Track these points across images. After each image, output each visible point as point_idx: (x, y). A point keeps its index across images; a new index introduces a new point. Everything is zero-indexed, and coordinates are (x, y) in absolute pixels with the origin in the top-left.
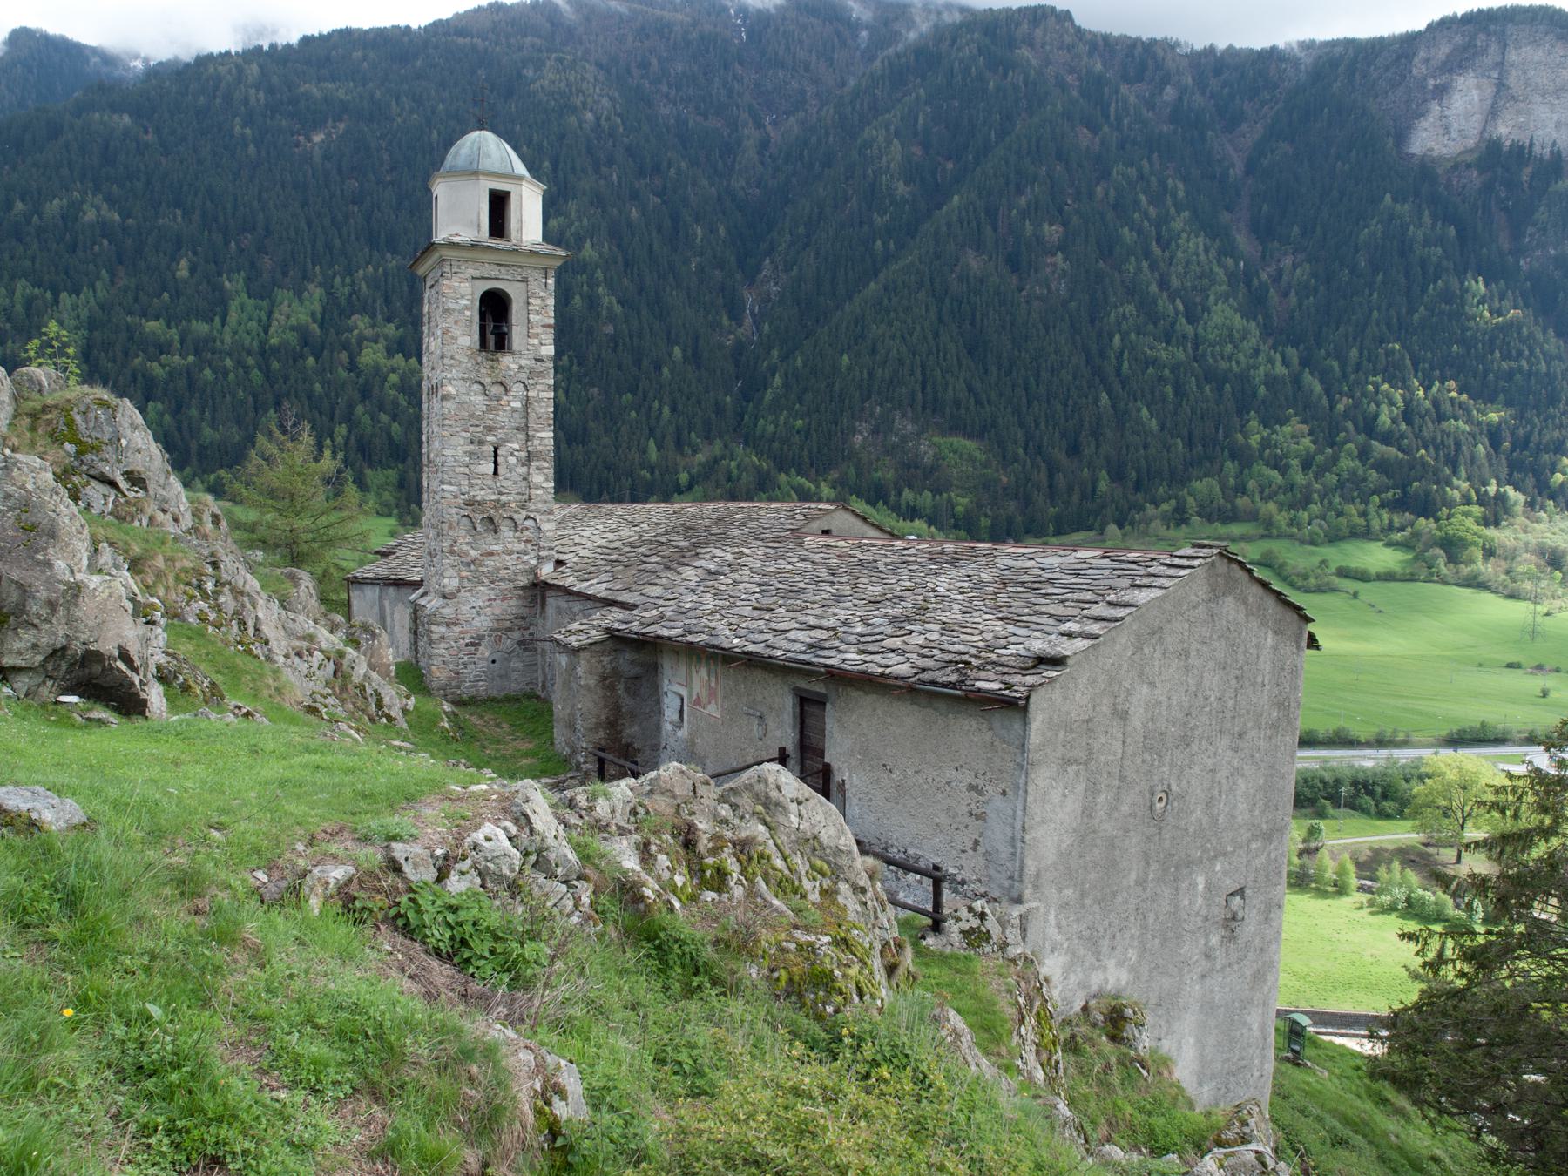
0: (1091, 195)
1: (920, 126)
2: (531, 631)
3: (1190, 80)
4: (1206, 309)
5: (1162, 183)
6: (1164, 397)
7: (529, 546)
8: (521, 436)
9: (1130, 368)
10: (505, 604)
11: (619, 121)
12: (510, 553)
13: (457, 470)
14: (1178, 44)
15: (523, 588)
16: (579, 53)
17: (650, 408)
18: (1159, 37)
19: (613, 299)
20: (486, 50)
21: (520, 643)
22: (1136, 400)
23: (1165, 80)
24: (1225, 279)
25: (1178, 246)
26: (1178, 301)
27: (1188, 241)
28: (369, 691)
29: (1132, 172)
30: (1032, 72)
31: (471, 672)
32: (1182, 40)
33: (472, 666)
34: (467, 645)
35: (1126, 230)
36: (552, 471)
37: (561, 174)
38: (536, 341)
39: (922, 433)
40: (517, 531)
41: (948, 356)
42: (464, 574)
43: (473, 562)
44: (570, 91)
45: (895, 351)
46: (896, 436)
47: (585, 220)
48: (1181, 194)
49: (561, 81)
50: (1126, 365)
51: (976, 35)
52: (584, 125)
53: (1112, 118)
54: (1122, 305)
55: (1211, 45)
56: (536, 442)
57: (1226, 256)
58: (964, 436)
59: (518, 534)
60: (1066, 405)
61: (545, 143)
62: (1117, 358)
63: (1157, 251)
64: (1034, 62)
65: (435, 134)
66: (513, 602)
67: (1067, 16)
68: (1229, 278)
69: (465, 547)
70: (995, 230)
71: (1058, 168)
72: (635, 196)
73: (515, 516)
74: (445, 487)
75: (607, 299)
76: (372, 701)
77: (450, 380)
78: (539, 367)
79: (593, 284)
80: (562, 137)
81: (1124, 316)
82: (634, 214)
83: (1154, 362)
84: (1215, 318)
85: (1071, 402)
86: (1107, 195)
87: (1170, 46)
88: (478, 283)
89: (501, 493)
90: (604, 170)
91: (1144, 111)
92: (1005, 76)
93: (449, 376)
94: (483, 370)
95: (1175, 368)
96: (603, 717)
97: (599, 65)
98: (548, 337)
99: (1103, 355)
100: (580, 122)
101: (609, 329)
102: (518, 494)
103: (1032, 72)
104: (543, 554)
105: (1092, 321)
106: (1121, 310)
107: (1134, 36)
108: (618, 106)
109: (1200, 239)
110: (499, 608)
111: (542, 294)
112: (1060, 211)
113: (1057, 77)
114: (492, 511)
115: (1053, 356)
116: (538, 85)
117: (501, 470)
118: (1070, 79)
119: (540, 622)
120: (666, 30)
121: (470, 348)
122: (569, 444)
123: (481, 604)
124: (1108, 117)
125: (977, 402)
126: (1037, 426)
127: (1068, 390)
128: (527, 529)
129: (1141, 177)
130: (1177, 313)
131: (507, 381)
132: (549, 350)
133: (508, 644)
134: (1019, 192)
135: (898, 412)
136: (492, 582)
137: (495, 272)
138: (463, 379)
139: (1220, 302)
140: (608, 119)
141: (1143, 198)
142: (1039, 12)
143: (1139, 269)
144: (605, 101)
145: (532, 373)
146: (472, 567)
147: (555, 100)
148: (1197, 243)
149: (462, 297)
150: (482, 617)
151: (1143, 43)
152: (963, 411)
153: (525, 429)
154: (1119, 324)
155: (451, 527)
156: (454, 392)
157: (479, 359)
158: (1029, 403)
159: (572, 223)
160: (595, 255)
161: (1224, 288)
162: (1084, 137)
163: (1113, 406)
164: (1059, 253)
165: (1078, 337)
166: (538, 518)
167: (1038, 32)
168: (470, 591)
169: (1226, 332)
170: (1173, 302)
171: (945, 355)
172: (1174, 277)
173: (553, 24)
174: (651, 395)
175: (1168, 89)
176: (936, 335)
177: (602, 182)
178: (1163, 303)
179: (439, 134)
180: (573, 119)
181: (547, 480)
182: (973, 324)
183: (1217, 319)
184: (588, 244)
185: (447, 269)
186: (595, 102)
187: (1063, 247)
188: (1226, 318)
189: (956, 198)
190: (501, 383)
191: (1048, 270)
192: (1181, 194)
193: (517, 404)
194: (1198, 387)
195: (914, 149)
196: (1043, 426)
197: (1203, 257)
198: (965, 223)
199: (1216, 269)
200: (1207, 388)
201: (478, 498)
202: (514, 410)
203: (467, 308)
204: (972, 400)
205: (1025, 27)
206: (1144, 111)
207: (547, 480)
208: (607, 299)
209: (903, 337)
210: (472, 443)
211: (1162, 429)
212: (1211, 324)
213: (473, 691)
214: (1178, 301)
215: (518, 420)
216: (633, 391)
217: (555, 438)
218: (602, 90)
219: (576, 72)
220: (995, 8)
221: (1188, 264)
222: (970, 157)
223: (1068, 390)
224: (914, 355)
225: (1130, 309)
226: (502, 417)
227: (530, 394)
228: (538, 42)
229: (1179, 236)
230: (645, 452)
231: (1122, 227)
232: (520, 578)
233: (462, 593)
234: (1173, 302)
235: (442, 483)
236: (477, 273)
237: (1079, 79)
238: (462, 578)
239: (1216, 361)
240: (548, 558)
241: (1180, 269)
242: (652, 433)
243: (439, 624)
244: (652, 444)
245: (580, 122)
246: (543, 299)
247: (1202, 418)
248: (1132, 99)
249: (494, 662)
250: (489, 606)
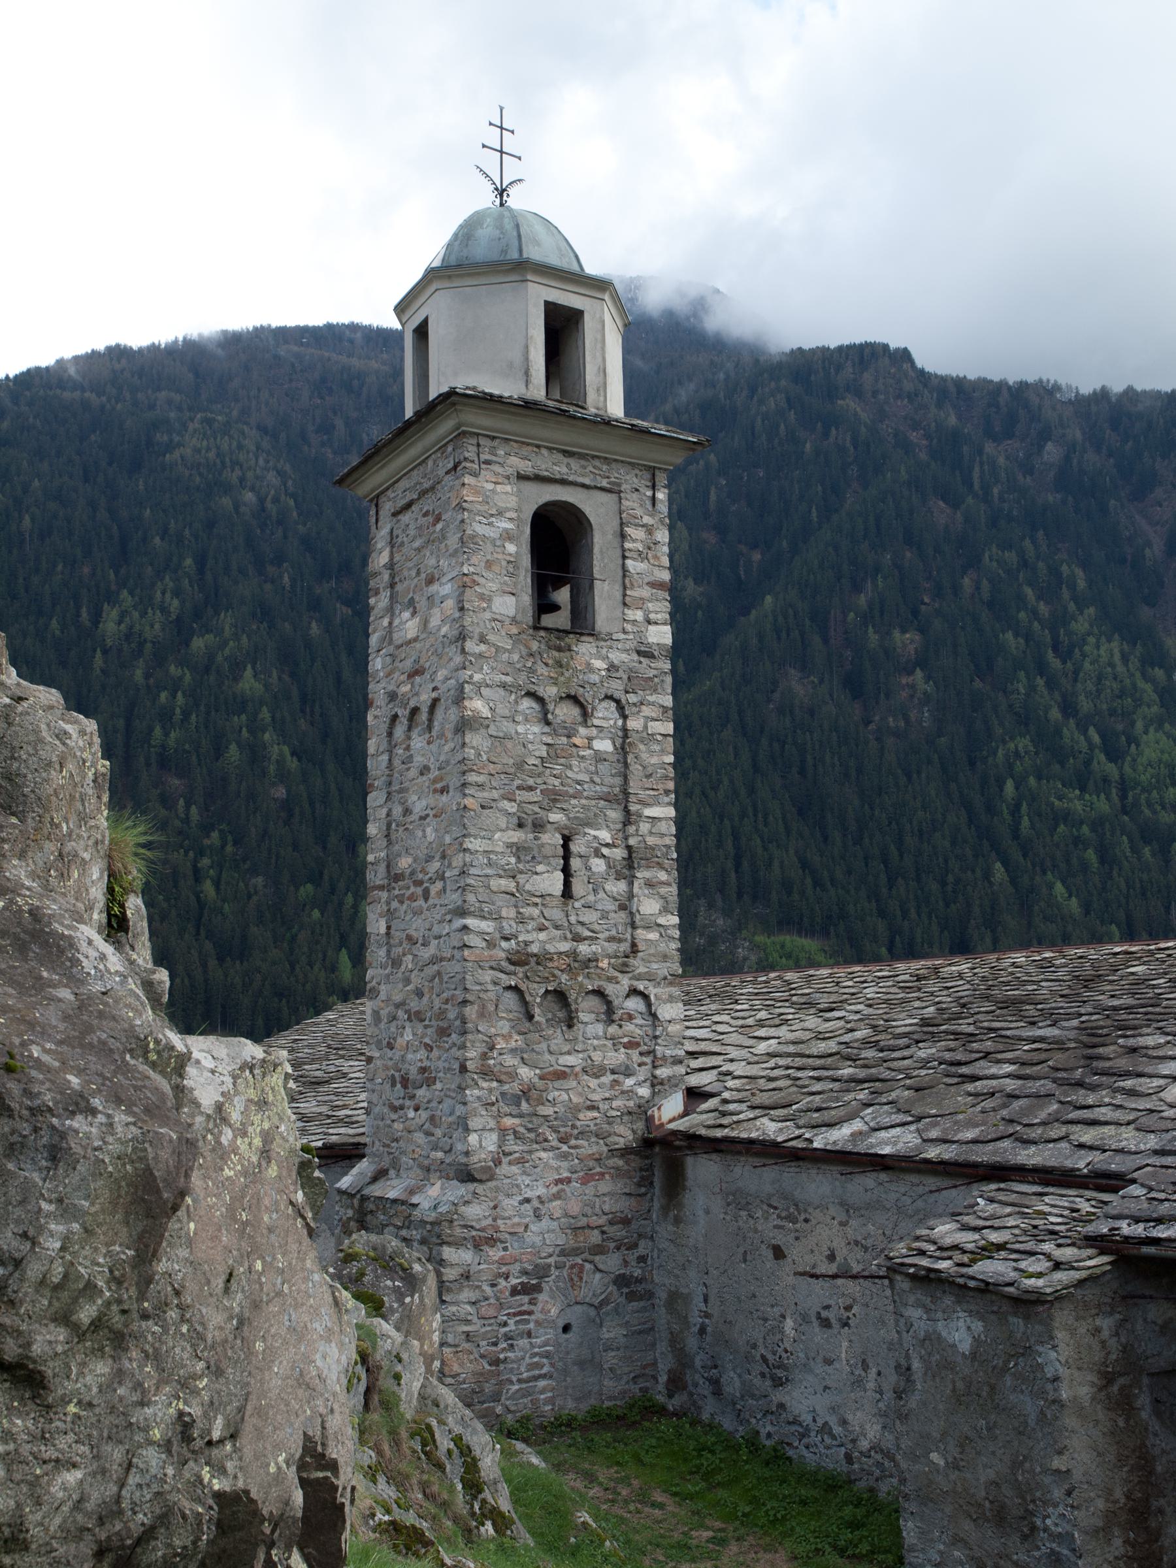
0: (956, 589)
1: (712, 505)
2: (641, 1251)
3: (1078, 435)
4: (1132, 740)
5: (1054, 571)
6: (1085, 867)
7: (635, 1054)
8: (615, 814)
9: (1033, 827)
10: (590, 1190)
11: (292, 503)
12: (596, 1071)
13: (495, 883)
14: (1057, 387)
15: (625, 1152)
16: (235, 413)
17: (341, 904)
18: (1031, 378)
19: (286, 749)
20: (103, 408)
21: (621, 1281)
22: (1044, 872)
23: (1045, 435)
24: (1155, 697)
25: (1084, 656)
26: (1092, 731)
27: (1098, 648)
28: (444, 1443)
29: (1011, 557)
30: (863, 430)
31: (522, 1355)
32: (1062, 382)
33: (523, 1342)
34: (514, 1292)
35: (1009, 635)
36: (674, 889)
37: (209, 577)
38: (639, 615)
39: (740, 930)
40: (611, 1022)
41: (771, 818)
42: (509, 1122)
43: (525, 1093)
44: (223, 463)
45: (694, 814)
46: (701, 935)
47: (244, 639)
48: (1081, 584)
49: (208, 449)
50: (1025, 822)
51: (783, 383)
52: (243, 509)
53: (977, 486)
54: (1012, 738)
55: (1103, 388)
56: (644, 827)
57: (1152, 666)
58: (799, 934)
59: (613, 1029)
60: (944, 884)
61: (187, 532)
62: (1012, 814)
63: (1054, 662)
64: (863, 416)
65: (27, 521)
66: (605, 1186)
67: (904, 355)
68: (1161, 697)
69: (510, 1061)
70: (826, 641)
71: (908, 554)
72: (315, 605)
73: (610, 989)
74: (470, 922)
75: (277, 750)
76: (454, 1469)
77: (479, 687)
78: (647, 668)
79: (255, 728)
80: (210, 525)
81: (1017, 754)
82: (315, 629)
83: (1066, 817)
84: (1147, 751)
85: (950, 878)
86: (978, 588)
87: (1045, 391)
88: (531, 488)
89: (577, 938)
90: (271, 570)
91: (1020, 477)
92: (826, 435)
93: (477, 677)
94: (542, 670)
95: (1097, 824)
96: (1118, 1494)
97: (263, 429)
98: (661, 608)
99: (990, 809)
100: (237, 507)
101: (280, 792)
102: (611, 939)
103: (863, 430)
104: (663, 1072)
105: (972, 763)
106: (1012, 746)
107: (996, 379)
108: (290, 483)
109: (1115, 644)
110: (575, 1201)
111: (647, 520)
112: (915, 613)
113: (896, 435)
114: (564, 978)
115: (920, 813)
116: (177, 454)
117: (578, 888)
118: (914, 436)
119: (665, 1230)
120: (356, 383)
121: (514, 620)
122: (221, 960)
123: (541, 1191)
124: (972, 485)
125: (817, 883)
126: (905, 914)
127: (946, 861)
128: (630, 1017)
129: (1024, 563)
130: (1091, 747)
131: (587, 696)
132: (662, 635)
133: (595, 1284)
134: (857, 588)
135: (702, 901)
136: (562, 1140)
137: (560, 467)
138: (504, 686)
139: (1152, 730)
140: (276, 500)
141: (1028, 591)
142: (867, 351)
143: (1032, 688)
144: (272, 477)
145: (634, 681)
146: (524, 1105)
147: (200, 475)
148: (1110, 651)
149: (500, 513)
150: (545, 1223)
151: (1009, 388)
152: (796, 897)
153: (623, 798)
154: (1011, 767)
155: (482, 1015)
156: (486, 712)
157: (535, 646)
158: (891, 883)
159: (225, 643)
160: (258, 687)
161: (1155, 709)
162: (940, 511)
163: (1013, 881)
164: (918, 671)
165: (953, 786)
166: (652, 991)
167: (867, 377)
168: (521, 1161)
169: (1164, 771)
170: (1085, 732)
171: (765, 817)
172: (1082, 697)
173: (197, 375)
174: (341, 885)
175: (1049, 446)
176: (752, 791)
177: (268, 587)
178: (1070, 732)
179: (33, 520)
180: (226, 501)
181: (665, 910)
182: (802, 772)
183: (1149, 753)
184: (249, 672)
185: (470, 453)
186: (257, 478)
187: (921, 661)
188: (1162, 752)
189: (769, 599)
190: (574, 699)
191: (904, 694)
192: (1081, 584)
193: (604, 745)
194: (1135, 850)
195: (705, 535)
196: (913, 914)
197: (1120, 668)
198: (784, 635)
199: (1141, 684)
200: (1147, 851)
201: (534, 948)
202: (599, 758)
203: (508, 536)
204: (809, 881)
205: (848, 371)
206: (1020, 477)
207: (665, 910)
208: (277, 750)
209: (703, 793)
210: (520, 825)
211: (1087, 913)
212: (1143, 760)
213: (523, 1406)
214: (1092, 731)
215: (609, 781)
216: (315, 878)
217: (680, 822)
218: (267, 462)
219: (231, 437)
220: (806, 347)
221: (1100, 678)
222: (785, 543)
223: (946, 861)
224: (722, 821)
225: (1024, 743)
226: (578, 772)
227: (632, 724)
228: (177, 398)
229: (1084, 641)
230: (333, 969)
231: (1003, 632)
232: (621, 1129)
233: (505, 1169)
234: (1085, 732)
235: (462, 912)
236: (526, 467)
237: (927, 436)
238: (503, 1132)
239: (1155, 812)
240: (671, 1083)
241: (1090, 686)
242: (343, 941)
243: (457, 1244)
244: (344, 956)
245: (237, 507)
246: (649, 530)
247: (1144, 894)
248: (1001, 460)
249: (566, 1329)
250: (557, 1196)
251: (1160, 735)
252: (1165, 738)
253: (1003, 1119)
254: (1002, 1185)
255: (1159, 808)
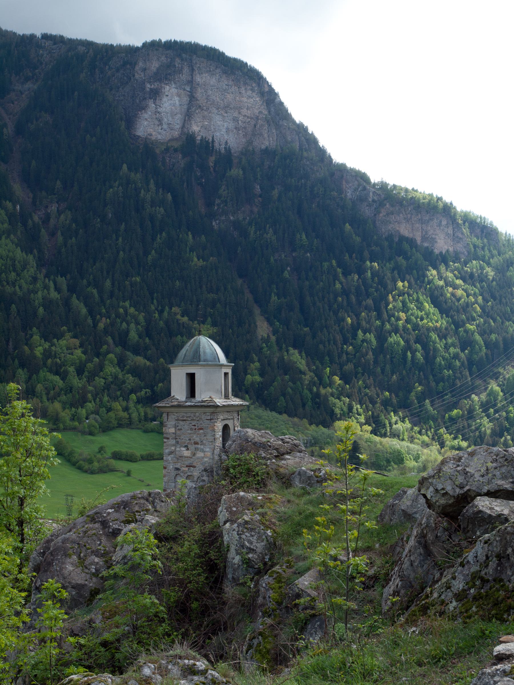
24: (6, 218)
188: (9, 251)
251: (8, 241)
252: (11, 243)
253: (194, 467)
254: (379, 472)
255: (5, 283)
